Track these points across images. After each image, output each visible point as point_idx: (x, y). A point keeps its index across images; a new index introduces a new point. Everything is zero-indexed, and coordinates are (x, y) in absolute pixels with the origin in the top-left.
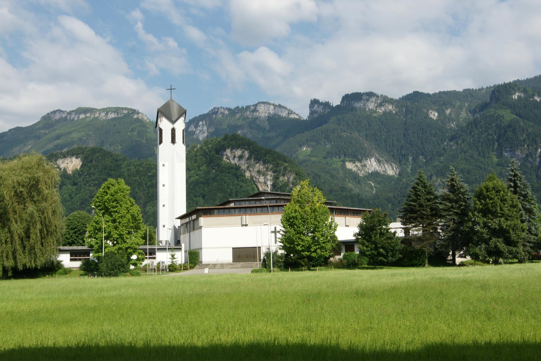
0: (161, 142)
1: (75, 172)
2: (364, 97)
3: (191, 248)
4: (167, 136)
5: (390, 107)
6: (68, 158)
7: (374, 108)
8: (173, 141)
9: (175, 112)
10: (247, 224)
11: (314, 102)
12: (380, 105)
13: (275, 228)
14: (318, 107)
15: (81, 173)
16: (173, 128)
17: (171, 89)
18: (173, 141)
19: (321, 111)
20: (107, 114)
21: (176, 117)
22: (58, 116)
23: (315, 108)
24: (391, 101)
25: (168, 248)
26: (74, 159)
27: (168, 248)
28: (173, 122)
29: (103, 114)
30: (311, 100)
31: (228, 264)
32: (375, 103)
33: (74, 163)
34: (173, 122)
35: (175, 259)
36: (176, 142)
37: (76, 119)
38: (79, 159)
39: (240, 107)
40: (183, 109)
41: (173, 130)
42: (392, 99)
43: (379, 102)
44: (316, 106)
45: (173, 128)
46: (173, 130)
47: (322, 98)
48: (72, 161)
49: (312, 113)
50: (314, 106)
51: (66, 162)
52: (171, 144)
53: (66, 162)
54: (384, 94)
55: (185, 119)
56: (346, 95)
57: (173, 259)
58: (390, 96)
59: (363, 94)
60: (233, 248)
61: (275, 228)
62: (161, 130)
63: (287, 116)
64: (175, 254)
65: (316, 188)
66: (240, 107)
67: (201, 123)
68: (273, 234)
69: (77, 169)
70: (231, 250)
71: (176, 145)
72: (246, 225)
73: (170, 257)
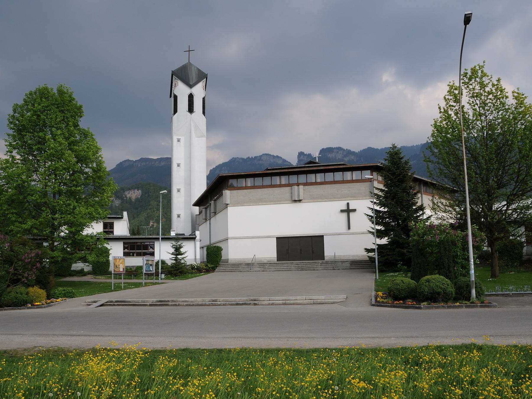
0: (175, 111)
1: (137, 200)
2: (335, 150)
3: (212, 242)
4: (183, 104)
5: (353, 157)
6: (132, 190)
7: (342, 158)
8: (191, 110)
9: (193, 76)
10: (301, 199)
11: (301, 154)
12: (345, 156)
13: (348, 204)
14: (303, 157)
15: (141, 200)
16: (191, 94)
17: (189, 51)
18: (191, 110)
19: (306, 160)
20: (160, 162)
21: (194, 81)
22: (127, 164)
23: (301, 158)
24: (353, 153)
25: (162, 238)
26: (136, 191)
27: (162, 238)
28: (191, 86)
29: (157, 162)
30: (299, 152)
31: (270, 264)
32: (343, 154)
33: (136, 194)
34: (191, 86)
35: (182, 254)
36: (194, 111)
37: (139, 165)
38: (140, 191)
39: (250, 157)
40: (203, 73)
41: (191, 97)
42: (354, 152)
43: (345, 153)
44: (302, 156)
45: (191, 94)
46: (191, 97)
47: (306, 152)
48: (134, 193)
49: (299, 161)
50: (301, 156)
51: (131, 193)
52: (188, 114)
53: (131, 193)
54: (349, 148)
55: (206, 86)
56: (322, 149)
57: (177, 255)
58: (352, 150)
59: (334, 148)
60: (276, 238)
61: (348, 204)
62: (176, 97)
63: (282, 163)
64: (182, 245)
65: (23, 392)
66: (250, 157)
67: (223, 168)
68: (345, 215)
69: (138, 198)
70: (274, 241)
71: (193, 114)
72: (300, 201)
73: (172, 250)
